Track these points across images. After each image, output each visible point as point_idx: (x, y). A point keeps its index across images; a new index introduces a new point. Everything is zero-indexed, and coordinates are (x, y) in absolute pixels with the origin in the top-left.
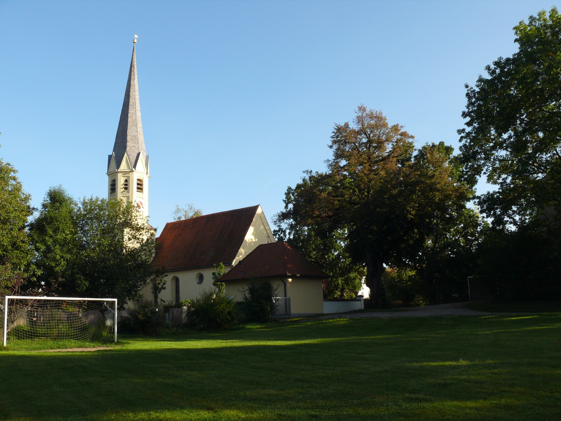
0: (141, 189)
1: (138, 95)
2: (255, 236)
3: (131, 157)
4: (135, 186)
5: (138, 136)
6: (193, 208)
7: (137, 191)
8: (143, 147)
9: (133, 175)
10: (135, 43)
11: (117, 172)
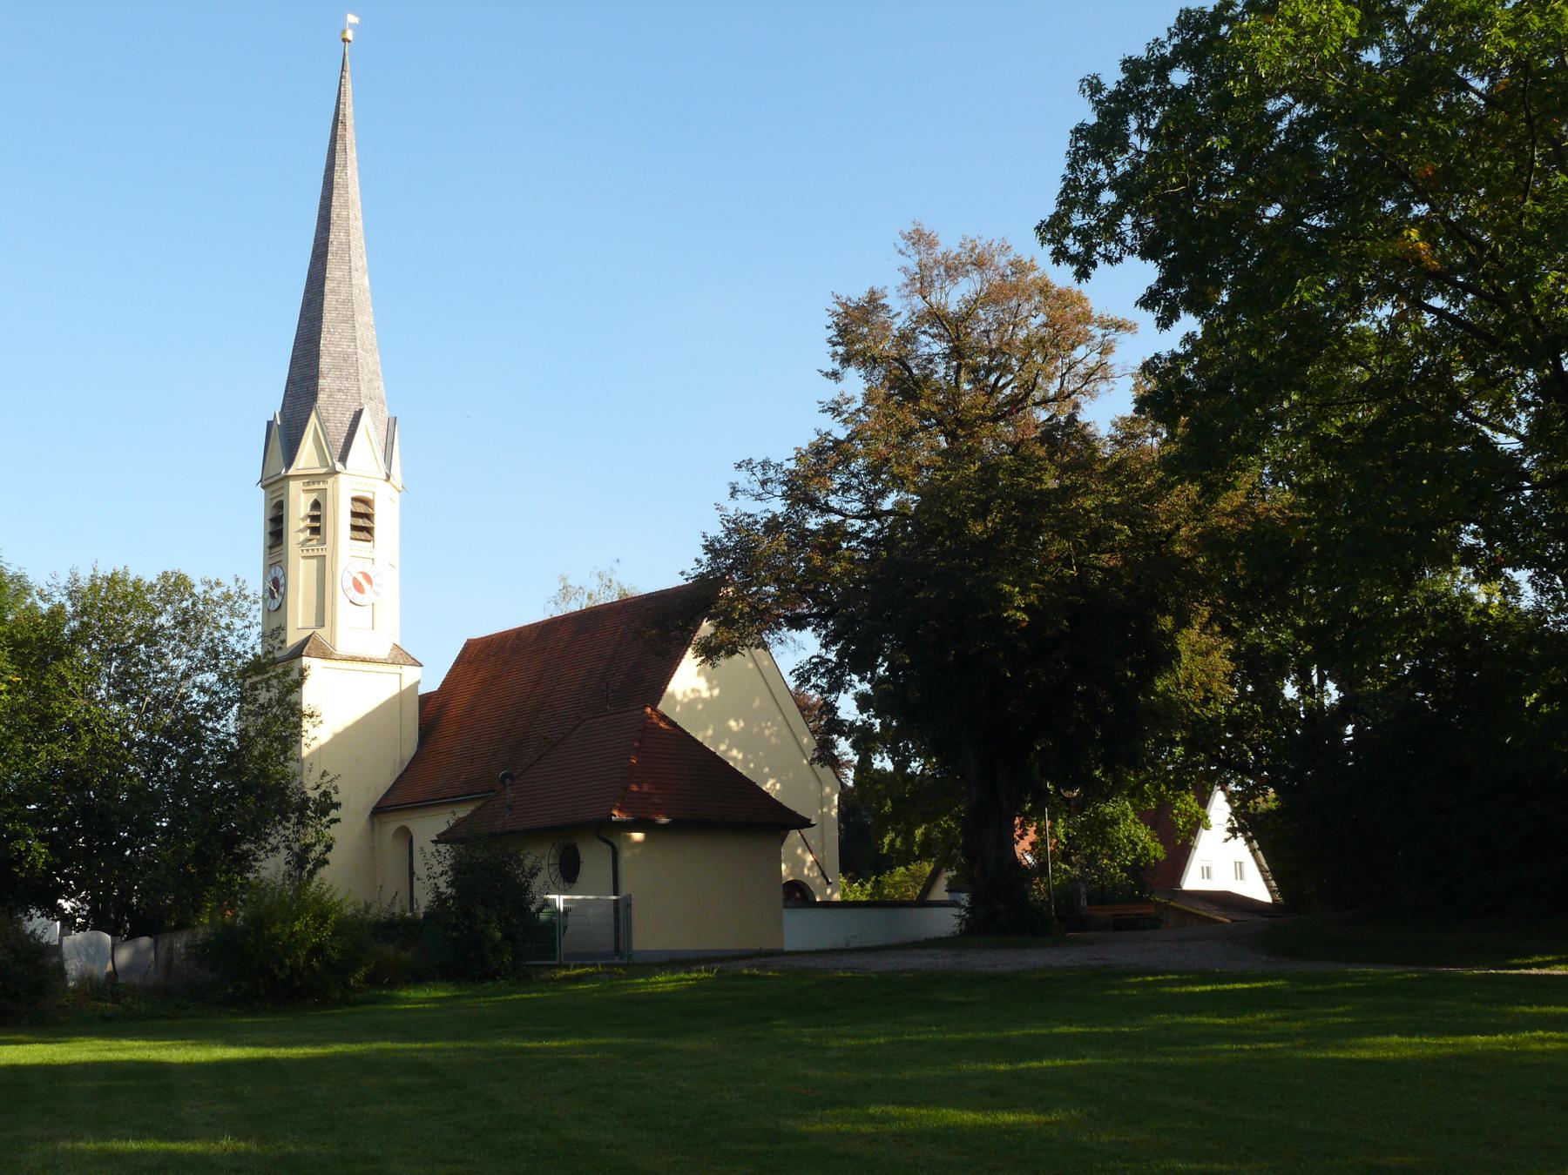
0: (369, 530)
1: (359, 215)
3: (330, 425)
4: (345, 521)
5: (356, 353)
6: (615, 585)
7: (351, 539)
9: (338, 487)
10: (349, 41)
11: (287, 478)
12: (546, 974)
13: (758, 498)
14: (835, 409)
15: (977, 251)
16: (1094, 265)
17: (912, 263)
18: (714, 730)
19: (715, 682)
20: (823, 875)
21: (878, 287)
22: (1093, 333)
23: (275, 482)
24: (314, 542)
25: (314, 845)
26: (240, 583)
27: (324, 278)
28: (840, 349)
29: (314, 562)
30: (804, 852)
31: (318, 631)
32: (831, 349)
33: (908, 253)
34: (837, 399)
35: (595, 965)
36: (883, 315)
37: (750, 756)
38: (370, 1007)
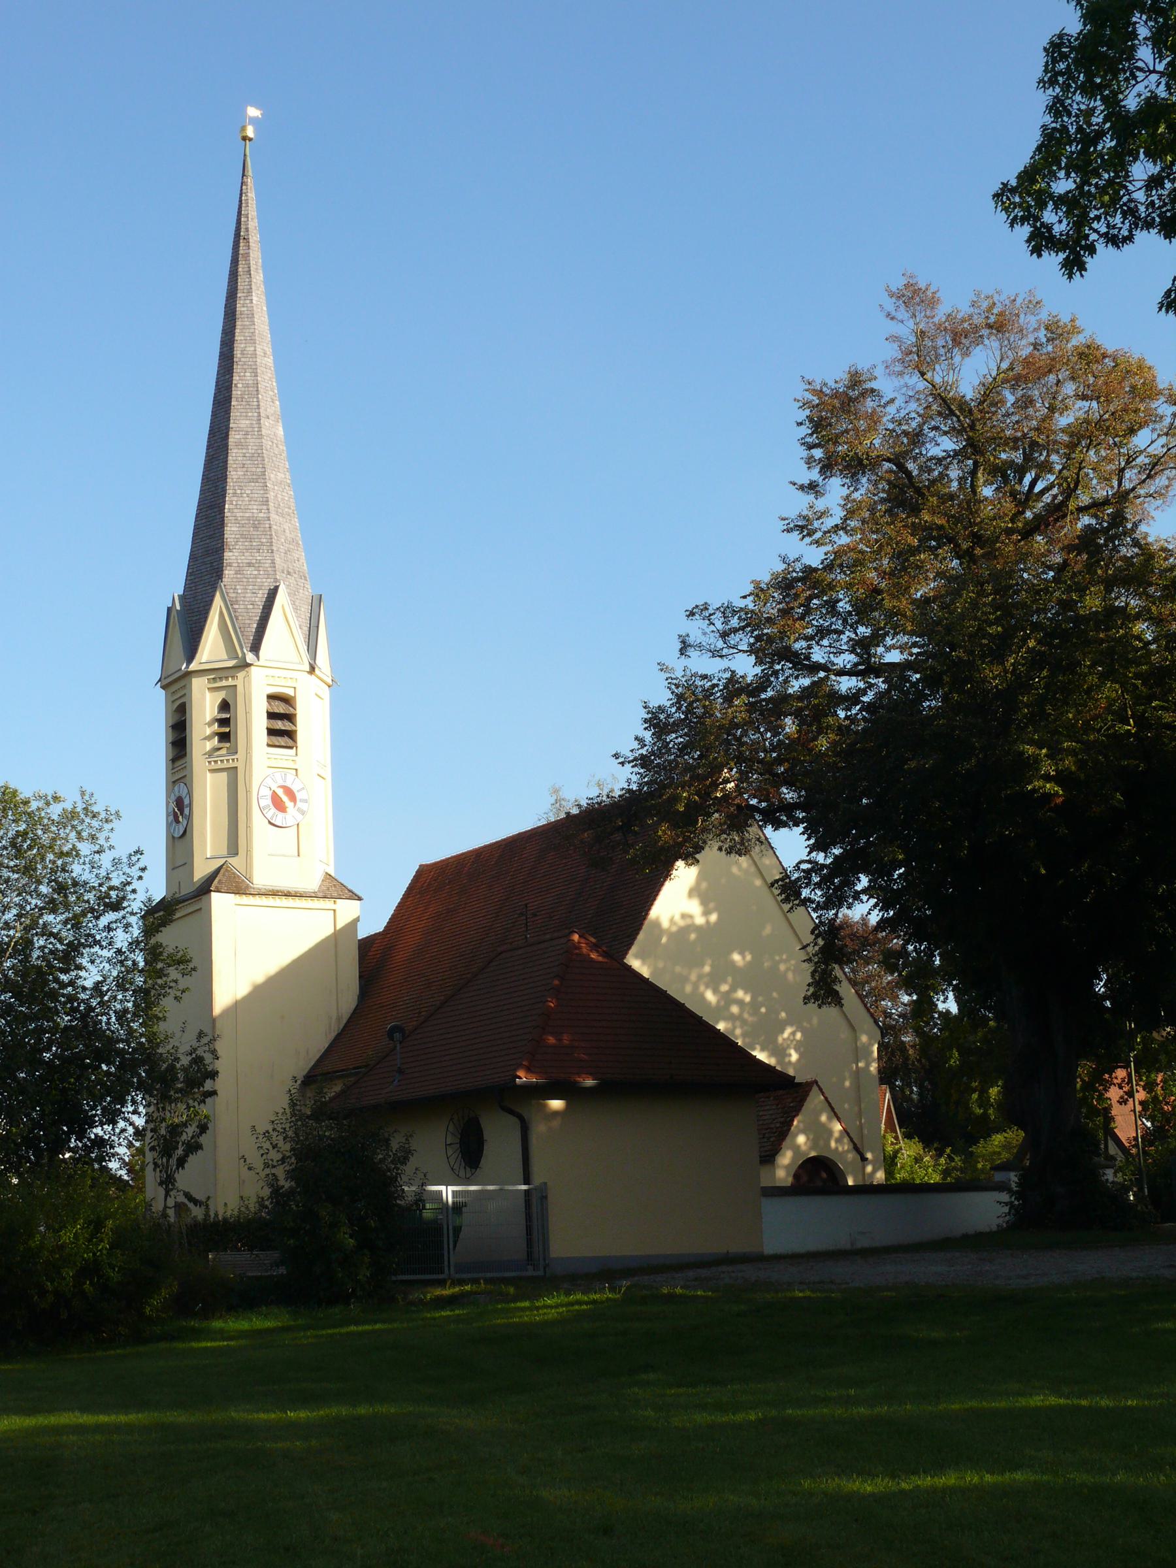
0: (290, 735)
1: (269, 351)
2: (704, 902)
4: (259, 723)
7: (269, 745)
8: (297, 564)
9: (250, 683)
10: (250, 140)
11: (188, 674)
12: (415, 1295)
13: (716, 654)
14: (804, 527)
15: (995, 311)
16: (1092, 250)
17: (906, 331)
18: (712, 966)
19: (712, 905)
20: (856, 1148)
21: (863, 365)
22: (1160, 411)
23: (175, 681)
24: (223, 751)
25: (185, 1125)
26: (87, 797)
27: (228, 428)
28: (818, 453)
29: (224, 775)
30: (829, 1119)
31: (230, 860)
32: (805, 454)
33: (899, 316)
34: (805, 513)
35: (475, 1281)
36: (869, 404)
37: (760, 999)
38: (163, 1345)
